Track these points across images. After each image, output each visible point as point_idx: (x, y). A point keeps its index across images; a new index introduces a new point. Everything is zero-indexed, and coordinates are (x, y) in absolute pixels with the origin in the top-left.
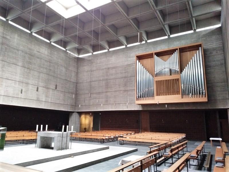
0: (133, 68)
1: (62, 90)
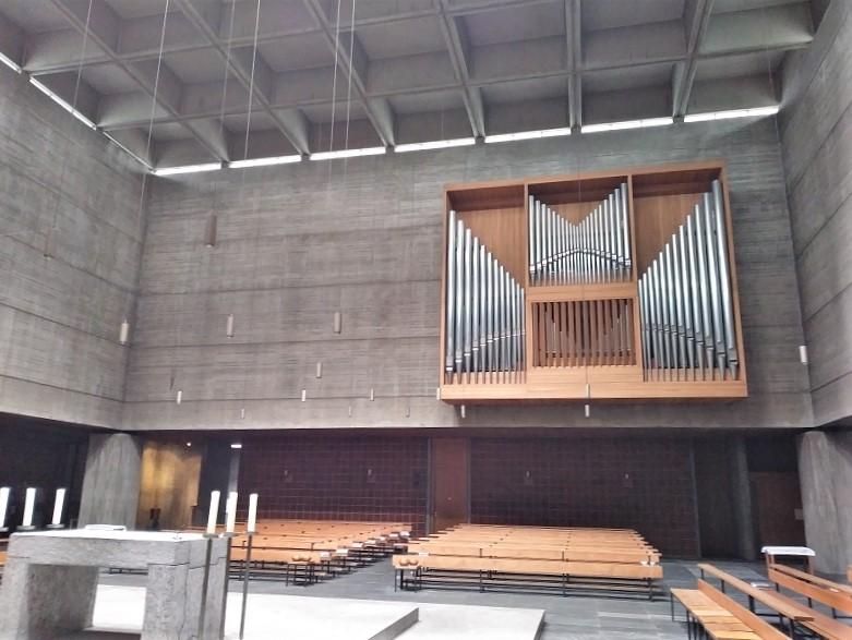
0: (420, 244)
1: (65, 319)
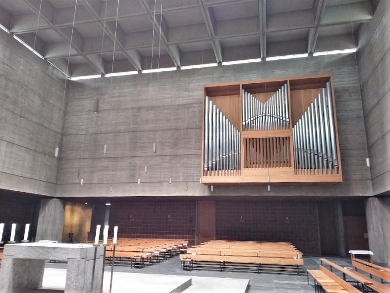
0: (192, 112)
1: (30, 146)
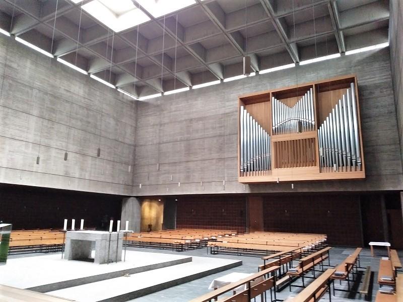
0: (233, 119)
1: (109, 158)
